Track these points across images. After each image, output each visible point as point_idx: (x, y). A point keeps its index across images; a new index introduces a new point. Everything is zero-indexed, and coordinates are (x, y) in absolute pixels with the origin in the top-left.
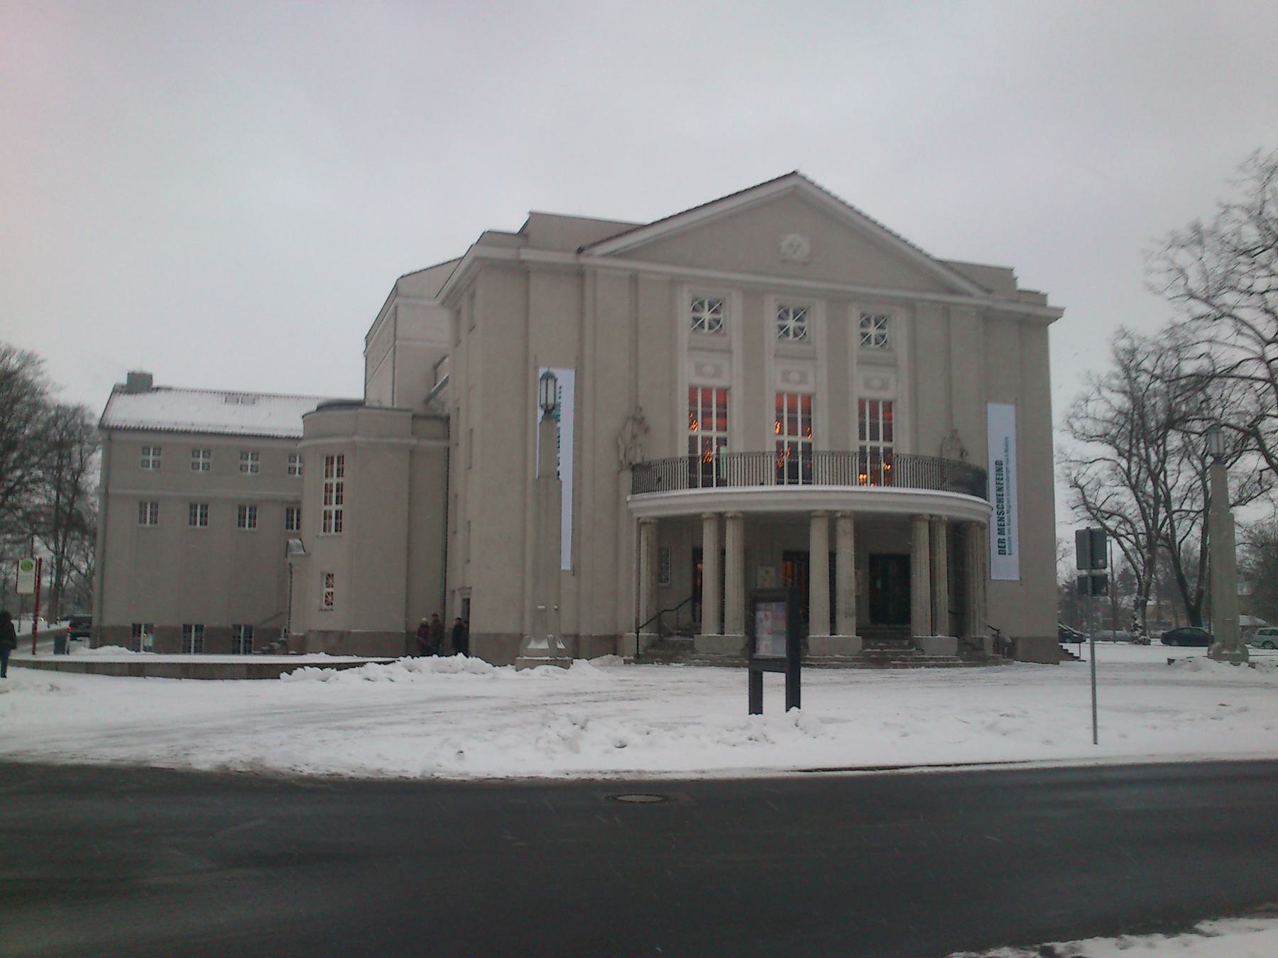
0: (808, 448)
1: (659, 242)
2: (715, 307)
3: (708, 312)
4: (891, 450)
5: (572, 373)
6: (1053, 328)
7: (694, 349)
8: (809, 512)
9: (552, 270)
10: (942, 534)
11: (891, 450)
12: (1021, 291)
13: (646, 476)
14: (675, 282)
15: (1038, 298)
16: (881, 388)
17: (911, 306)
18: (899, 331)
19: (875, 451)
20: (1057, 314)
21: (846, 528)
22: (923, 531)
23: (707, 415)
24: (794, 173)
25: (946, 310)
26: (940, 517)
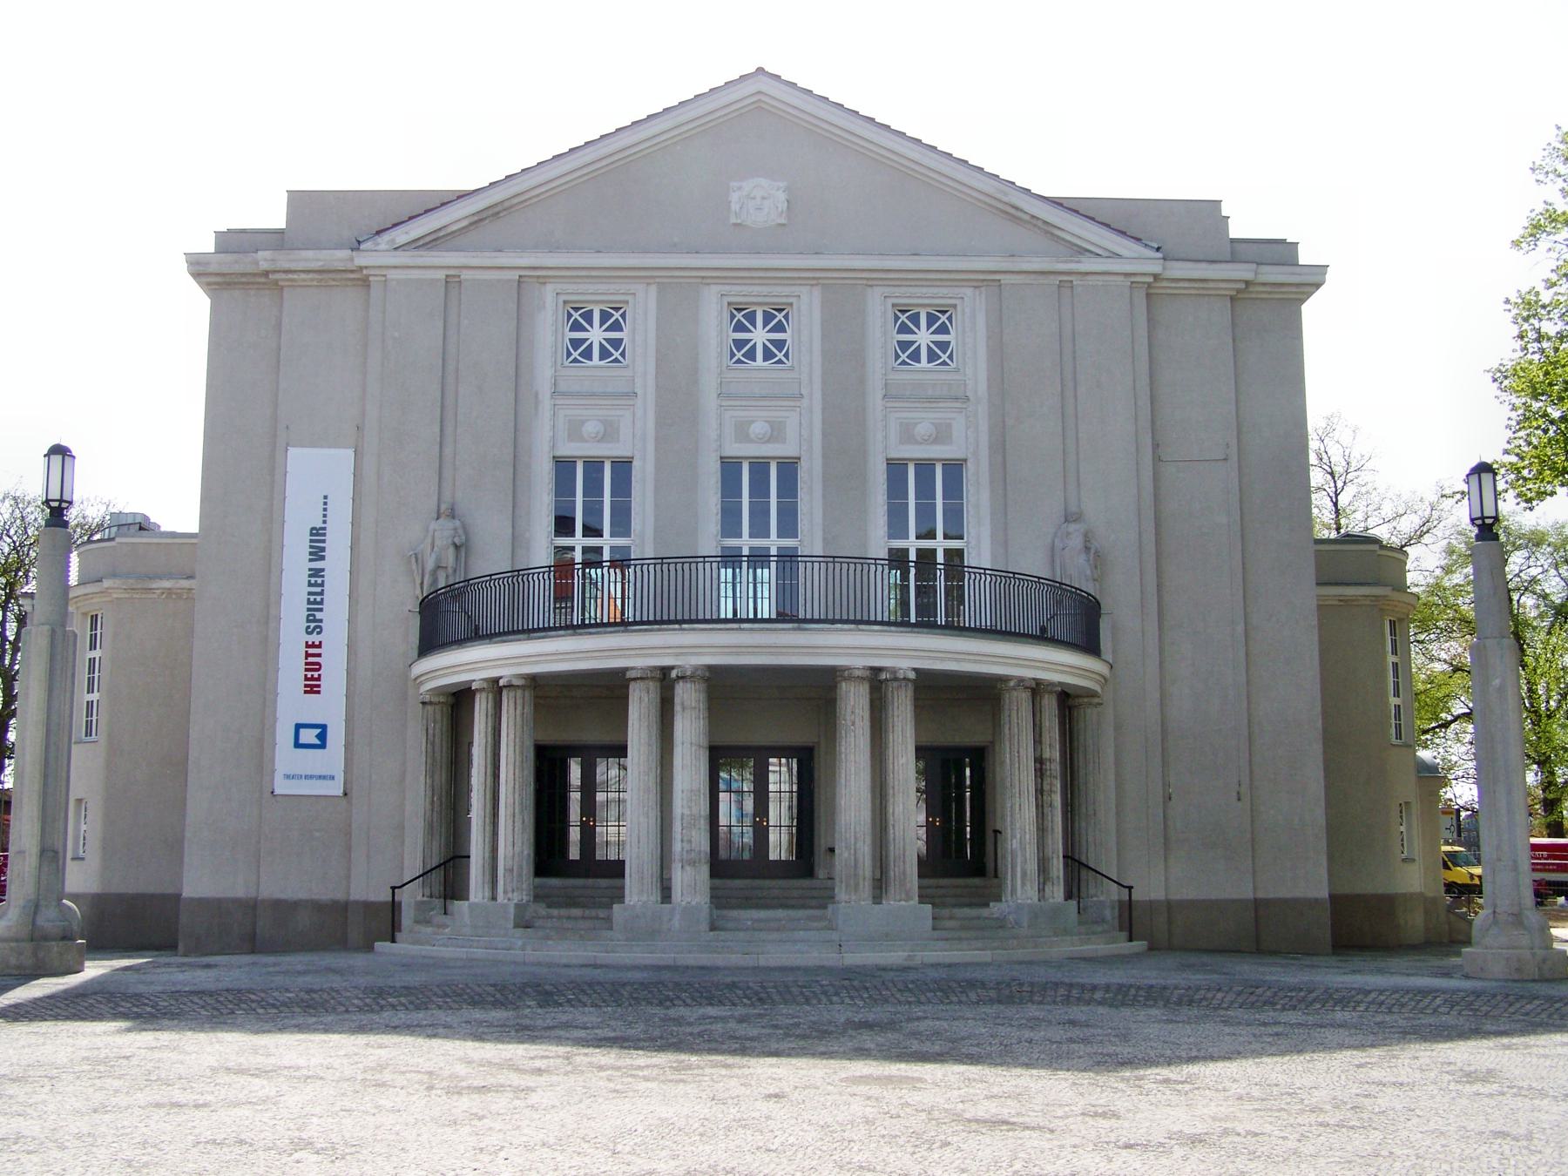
0: (954, 556)
1: (494, 213)
2: (939, 320)
3: (594, 328)
4: (959, 553)
5: (351, 453)
6: (1311, 311)
7: (729, 397)
8: (622, 672)
9: (326, 276)
10: (1050, 705)
11: (959, 553)
12: (1233, 241)
13: (442, 619)
14: (524, 283)
15: (1281, 252)
16: (770, 440)
17: (988, 282)
18: (970, 335)
19: (926, 557)
20: (1313, 280)
21: (688, 697)
22: (854, 704)
23: (926, 512)
24: (760, 70)
25: (1065, 283)
26: (894, 671)
